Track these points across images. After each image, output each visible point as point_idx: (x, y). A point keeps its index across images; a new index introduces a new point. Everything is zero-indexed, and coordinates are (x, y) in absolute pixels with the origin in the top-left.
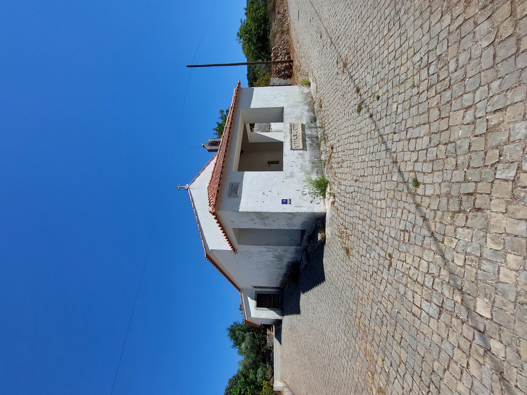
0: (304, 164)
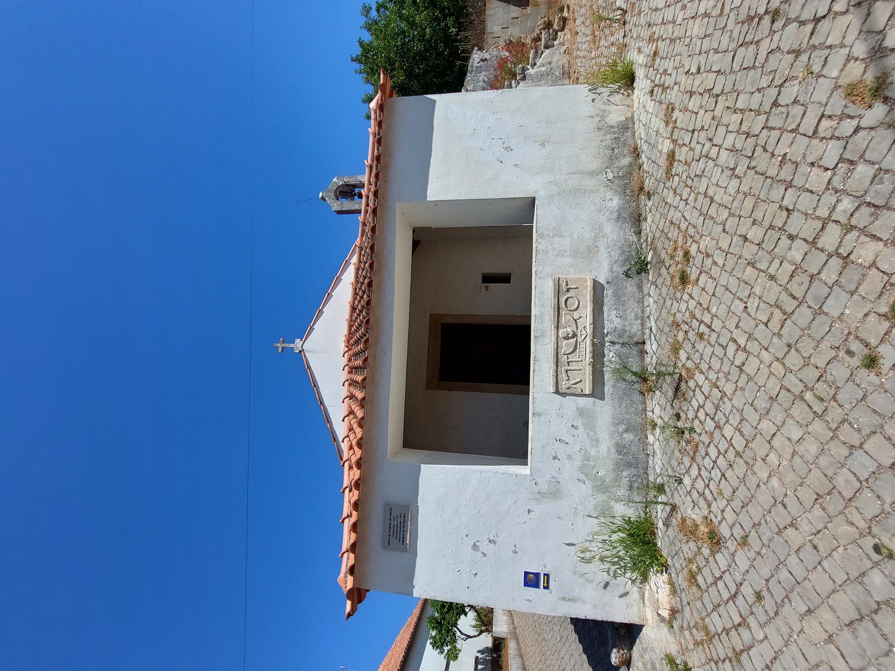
0: (593, 452)
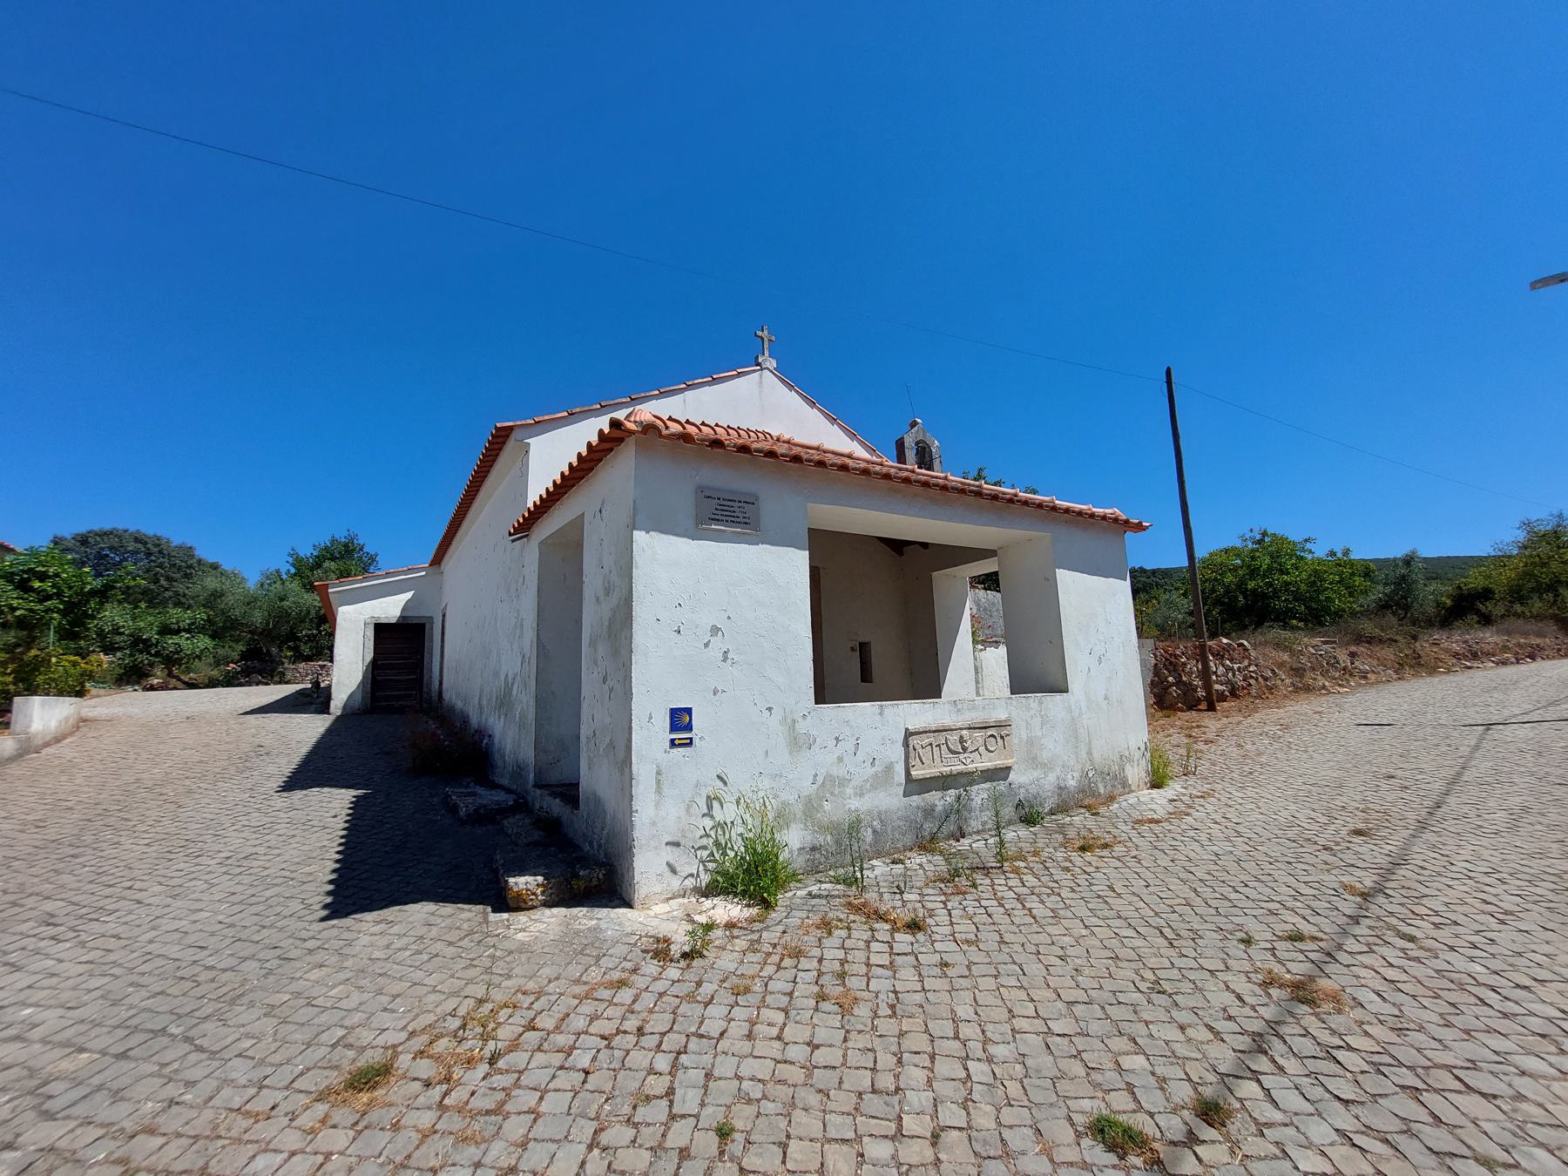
0: (849, 791)
